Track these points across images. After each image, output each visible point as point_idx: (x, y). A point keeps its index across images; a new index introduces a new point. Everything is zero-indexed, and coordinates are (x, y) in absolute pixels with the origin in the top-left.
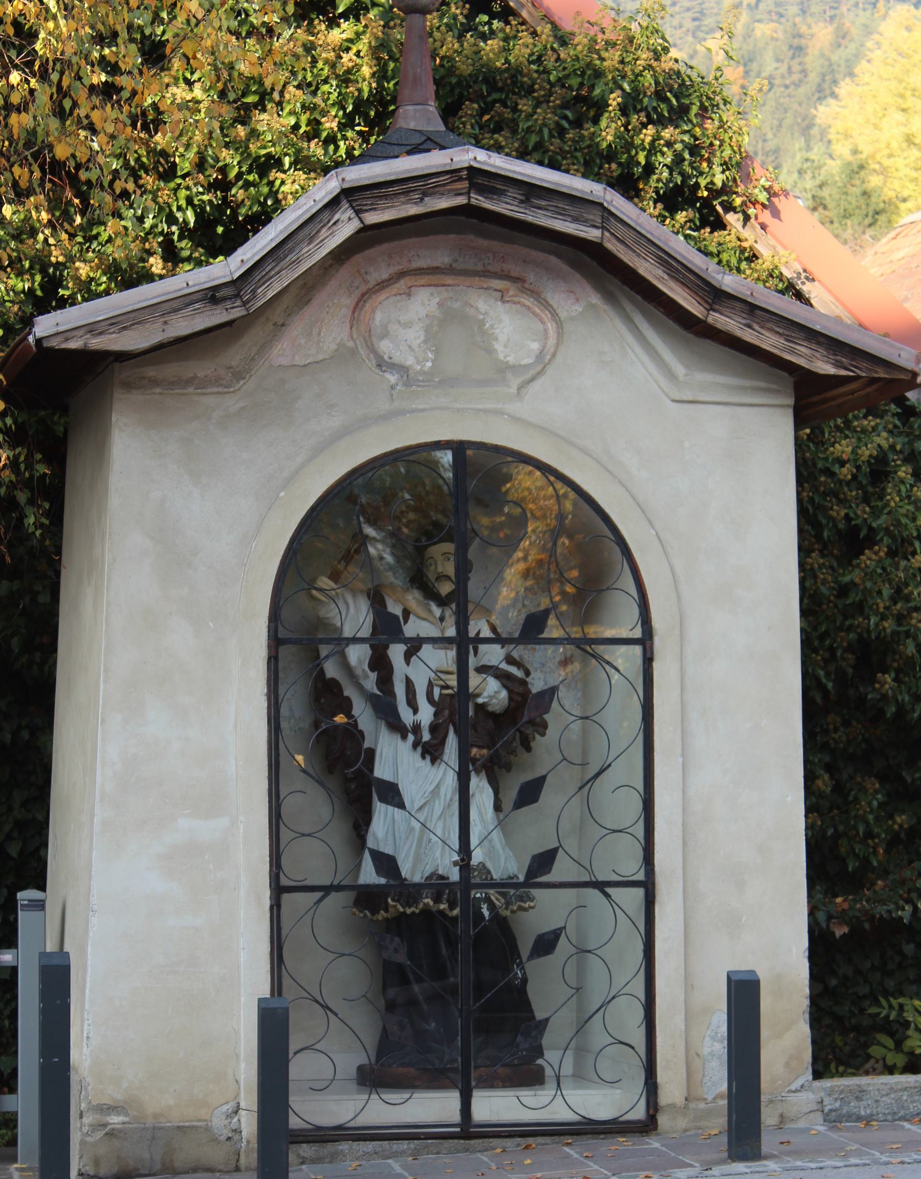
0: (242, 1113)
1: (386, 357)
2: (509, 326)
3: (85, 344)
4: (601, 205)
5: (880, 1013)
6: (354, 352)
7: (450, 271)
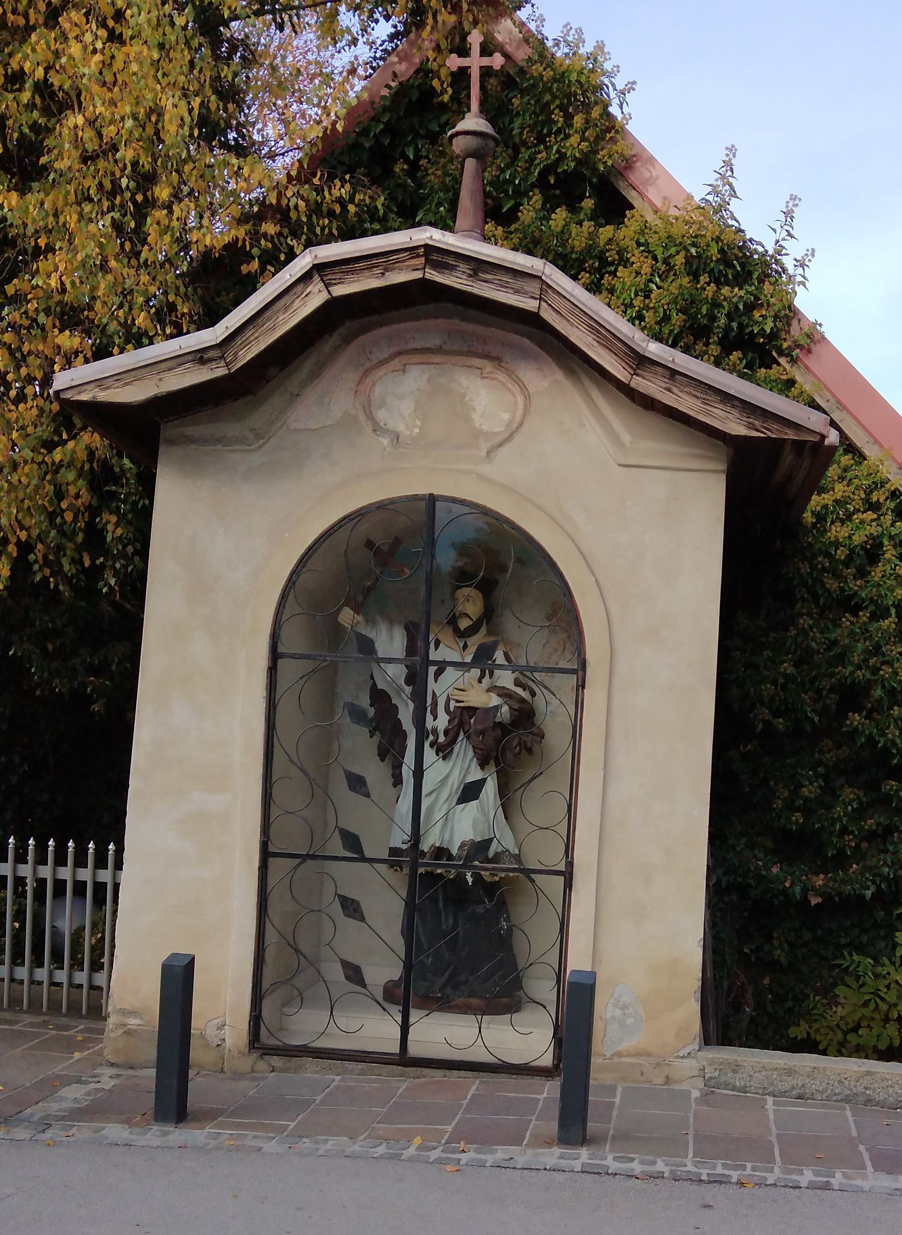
0: (226, 1027)
1: (382, 424)
2: (485, 397)
3: (94, 397)
4: (540, 278)
5: (842, 965)
6: (355, 419)
7: (438, 350)
